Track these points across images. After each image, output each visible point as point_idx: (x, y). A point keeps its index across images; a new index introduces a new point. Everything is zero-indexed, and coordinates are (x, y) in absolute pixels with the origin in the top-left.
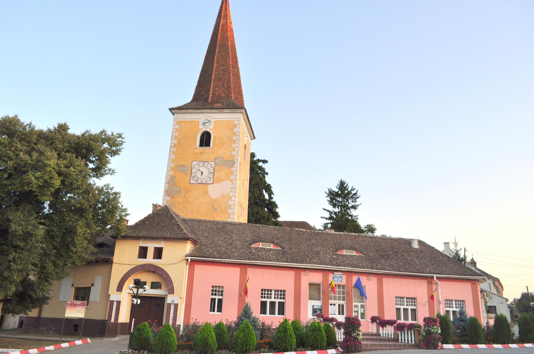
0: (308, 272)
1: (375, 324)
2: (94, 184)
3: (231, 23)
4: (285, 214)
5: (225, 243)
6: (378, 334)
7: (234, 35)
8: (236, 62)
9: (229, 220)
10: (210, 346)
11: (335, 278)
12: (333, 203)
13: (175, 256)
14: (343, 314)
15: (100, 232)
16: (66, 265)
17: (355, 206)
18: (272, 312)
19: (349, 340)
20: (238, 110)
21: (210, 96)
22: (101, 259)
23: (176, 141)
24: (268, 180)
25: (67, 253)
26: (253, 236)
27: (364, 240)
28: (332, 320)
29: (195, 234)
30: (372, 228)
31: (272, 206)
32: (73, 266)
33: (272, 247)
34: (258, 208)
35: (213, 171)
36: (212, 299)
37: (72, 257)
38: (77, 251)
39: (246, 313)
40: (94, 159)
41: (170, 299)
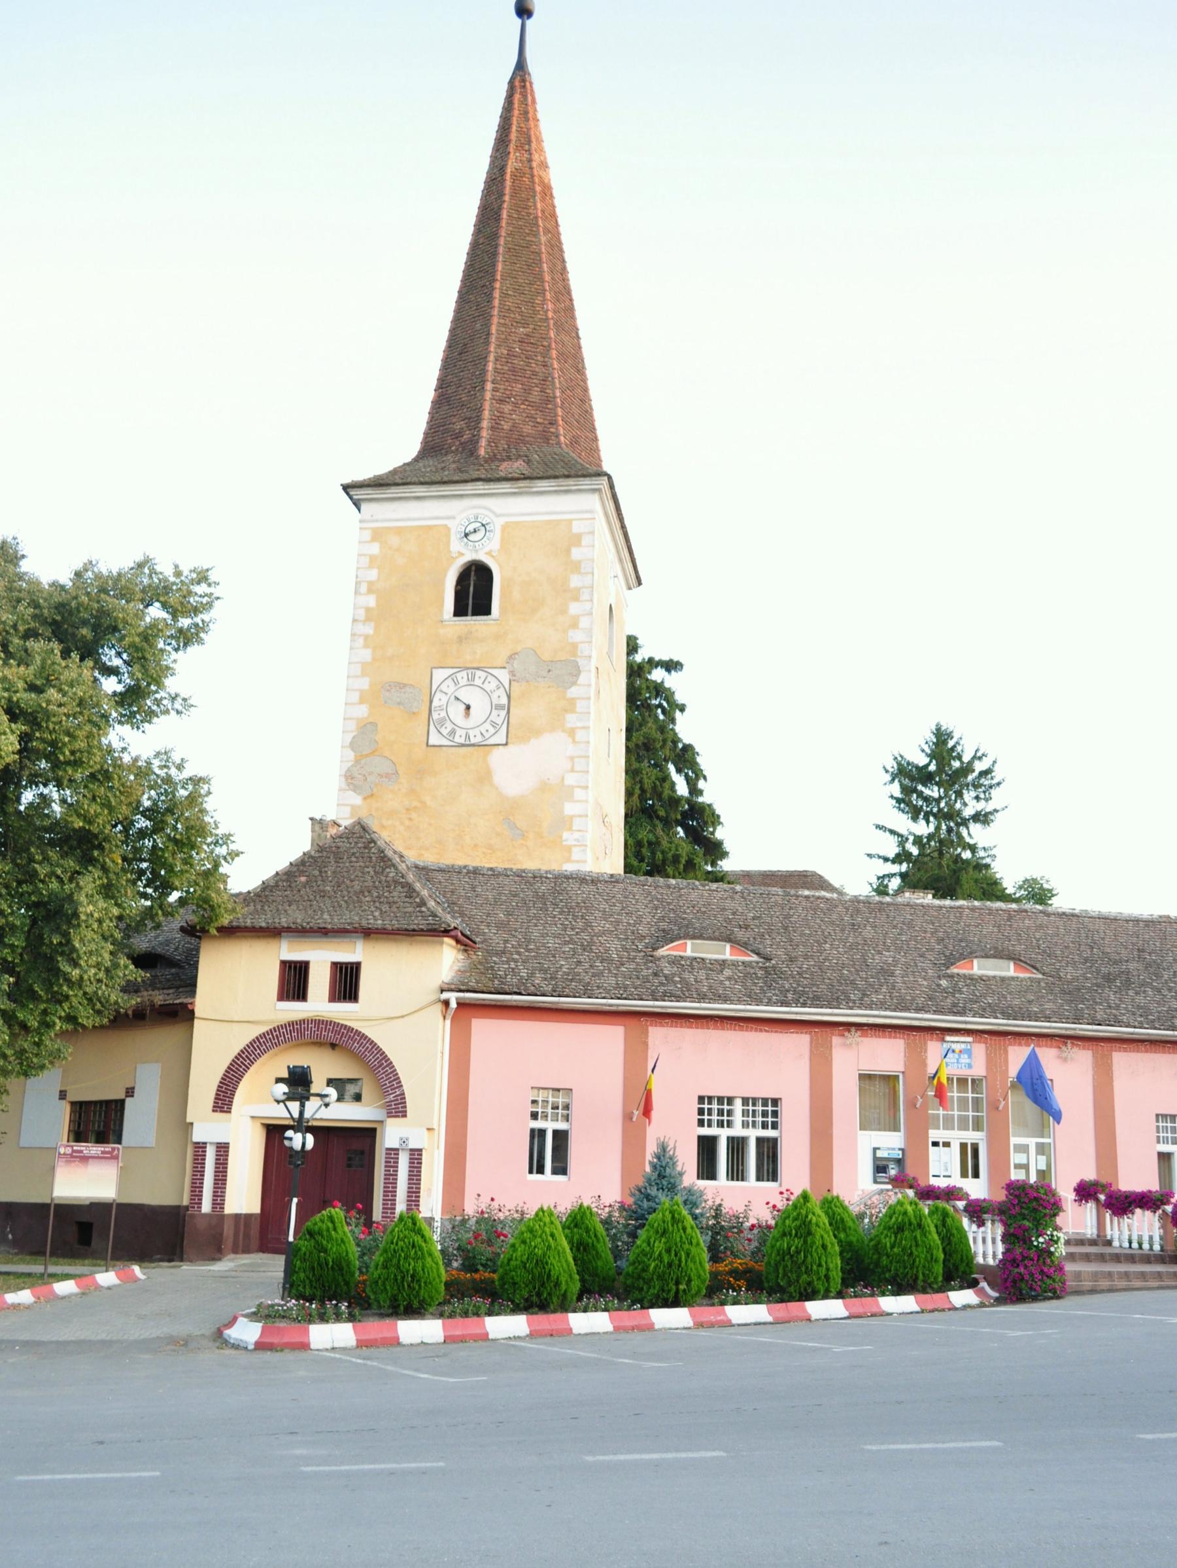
0: (854, 1037)
1: (1091, 1206)
2: (124, 749)
3: (544, 165)
4: (746, 846)
5: (566, 943)
6: (1102, 1240)
7: (558, 211)
8: (570, 310)
9: (569, 868)
10: (557, 1284)
11: (950, 1055)
12: (909, 804)
13: (404, 989)
14: (976, 1175)
15: (149, 913)
16: (49, 1026)
17: (986, 815)
18: (737, 1172)
19: (1024, 1258)
20: (586, 483)
21: (484, 433)
22: (152, 1005)
23: (371, 601)
24: (686, 729)
25: (51, 985)
26: (662, 919)
27: (1041, 927)
28: (951, 1194)
29: (462, 915)
30: (1041, 888)
31: (698, 820)
32: (70, 1027)
33: (726, 952)
34: (654, 826)
35: (504, 701)
36: (532, 1131)
37: (67, 997)
38: (81, 978)
39: (661, 1176)
40: (117, 662)
41: (392, 1135)
